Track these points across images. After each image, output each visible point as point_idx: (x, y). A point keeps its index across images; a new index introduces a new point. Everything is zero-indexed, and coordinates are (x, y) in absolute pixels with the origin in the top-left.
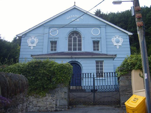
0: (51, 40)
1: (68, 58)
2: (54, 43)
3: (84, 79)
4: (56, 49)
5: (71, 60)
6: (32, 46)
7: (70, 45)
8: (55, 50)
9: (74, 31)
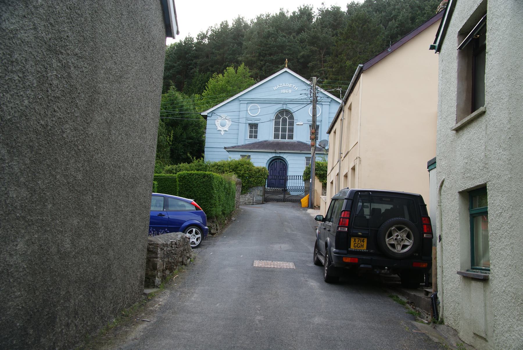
0: (250, 122)
1: (271, 152)
2: (254, 127)
3: (289, 180)
4: (257, 131)
5: (274, 155)
6: (223, 130)
7: (276, 130)
8: (256, 137)
9: (284, 109)
